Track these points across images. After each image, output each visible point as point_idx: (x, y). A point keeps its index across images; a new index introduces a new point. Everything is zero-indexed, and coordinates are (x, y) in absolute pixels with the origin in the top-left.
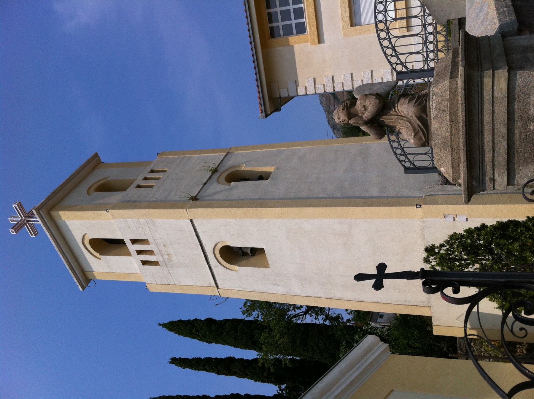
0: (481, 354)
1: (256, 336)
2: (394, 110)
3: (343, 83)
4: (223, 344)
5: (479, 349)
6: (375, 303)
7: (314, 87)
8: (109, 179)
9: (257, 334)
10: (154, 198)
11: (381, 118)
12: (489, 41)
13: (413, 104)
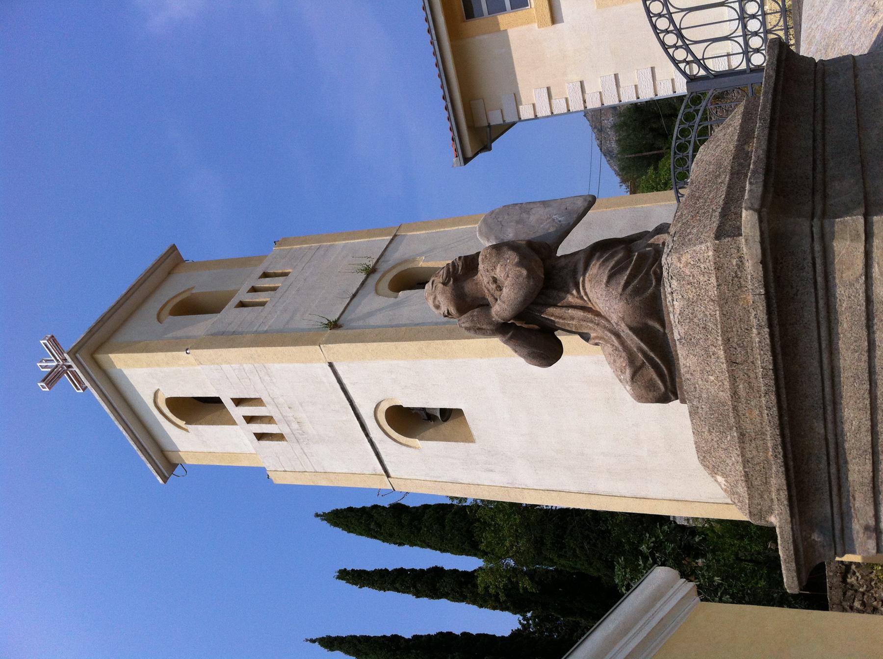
0: (870, 584)
1: (477, 533)
2: (574, 292)
3: (600, 93)
4: (422, 547)
5: (867, 575)
6: (670, 500)
7: (548, 102)
8: (194, 291)
9: (479, 529)
10: (266, 326)
11: (542, 313)
12: (856, 76)
13: (620, 290)
